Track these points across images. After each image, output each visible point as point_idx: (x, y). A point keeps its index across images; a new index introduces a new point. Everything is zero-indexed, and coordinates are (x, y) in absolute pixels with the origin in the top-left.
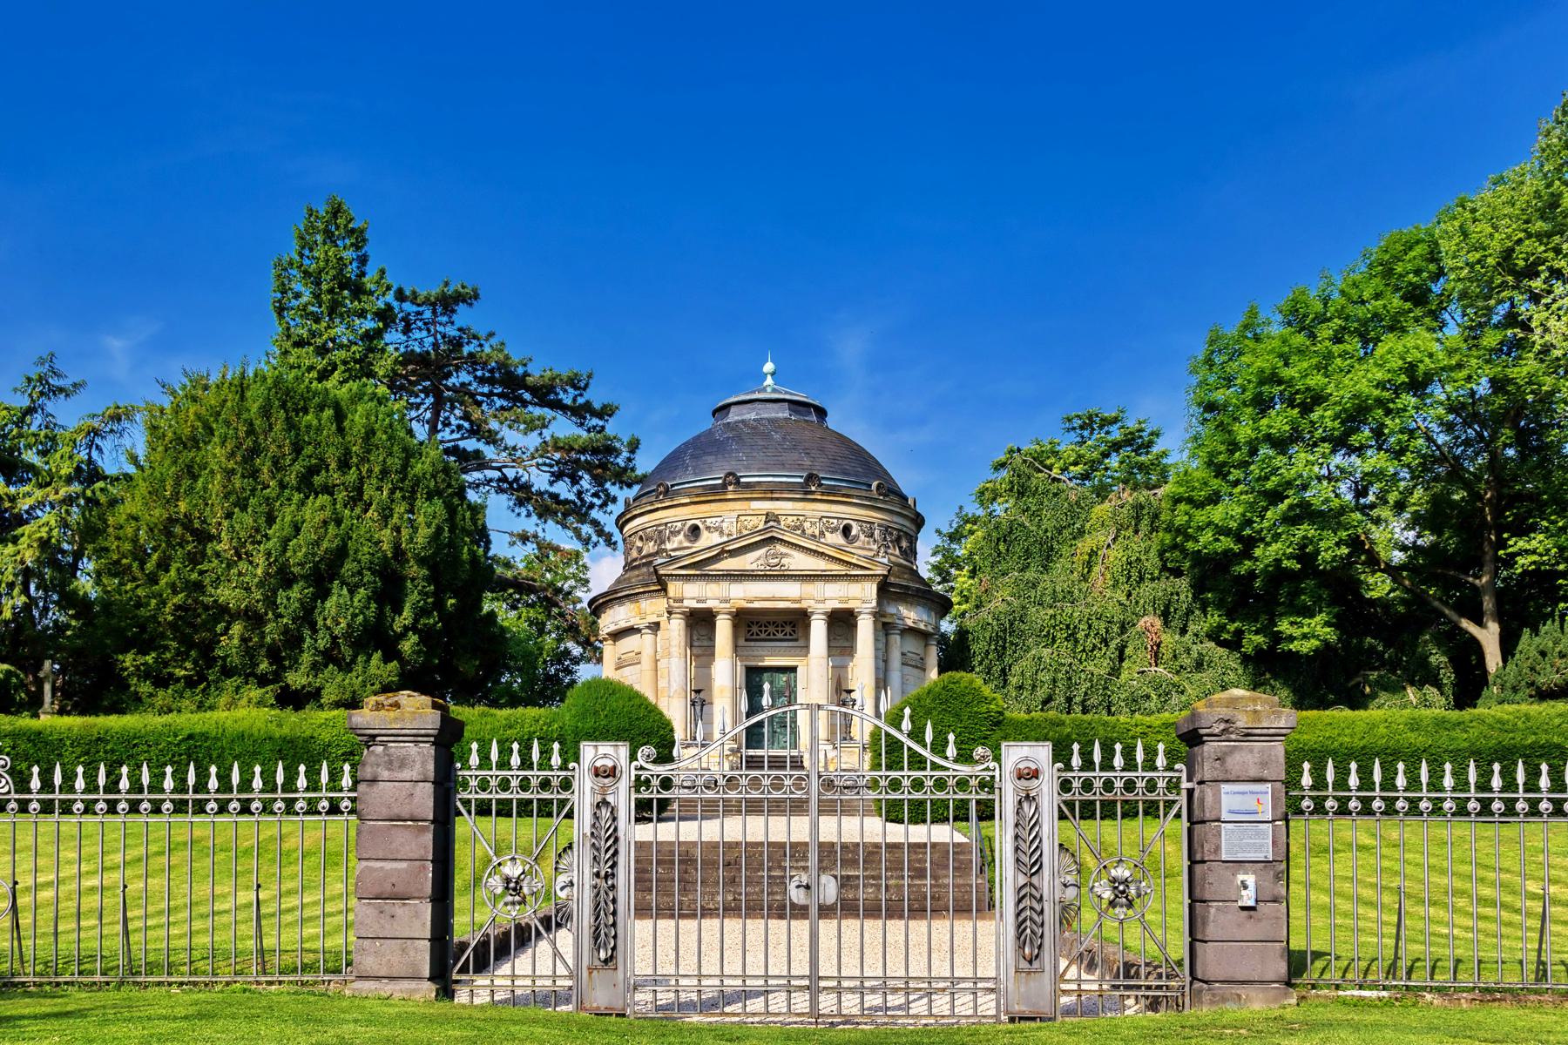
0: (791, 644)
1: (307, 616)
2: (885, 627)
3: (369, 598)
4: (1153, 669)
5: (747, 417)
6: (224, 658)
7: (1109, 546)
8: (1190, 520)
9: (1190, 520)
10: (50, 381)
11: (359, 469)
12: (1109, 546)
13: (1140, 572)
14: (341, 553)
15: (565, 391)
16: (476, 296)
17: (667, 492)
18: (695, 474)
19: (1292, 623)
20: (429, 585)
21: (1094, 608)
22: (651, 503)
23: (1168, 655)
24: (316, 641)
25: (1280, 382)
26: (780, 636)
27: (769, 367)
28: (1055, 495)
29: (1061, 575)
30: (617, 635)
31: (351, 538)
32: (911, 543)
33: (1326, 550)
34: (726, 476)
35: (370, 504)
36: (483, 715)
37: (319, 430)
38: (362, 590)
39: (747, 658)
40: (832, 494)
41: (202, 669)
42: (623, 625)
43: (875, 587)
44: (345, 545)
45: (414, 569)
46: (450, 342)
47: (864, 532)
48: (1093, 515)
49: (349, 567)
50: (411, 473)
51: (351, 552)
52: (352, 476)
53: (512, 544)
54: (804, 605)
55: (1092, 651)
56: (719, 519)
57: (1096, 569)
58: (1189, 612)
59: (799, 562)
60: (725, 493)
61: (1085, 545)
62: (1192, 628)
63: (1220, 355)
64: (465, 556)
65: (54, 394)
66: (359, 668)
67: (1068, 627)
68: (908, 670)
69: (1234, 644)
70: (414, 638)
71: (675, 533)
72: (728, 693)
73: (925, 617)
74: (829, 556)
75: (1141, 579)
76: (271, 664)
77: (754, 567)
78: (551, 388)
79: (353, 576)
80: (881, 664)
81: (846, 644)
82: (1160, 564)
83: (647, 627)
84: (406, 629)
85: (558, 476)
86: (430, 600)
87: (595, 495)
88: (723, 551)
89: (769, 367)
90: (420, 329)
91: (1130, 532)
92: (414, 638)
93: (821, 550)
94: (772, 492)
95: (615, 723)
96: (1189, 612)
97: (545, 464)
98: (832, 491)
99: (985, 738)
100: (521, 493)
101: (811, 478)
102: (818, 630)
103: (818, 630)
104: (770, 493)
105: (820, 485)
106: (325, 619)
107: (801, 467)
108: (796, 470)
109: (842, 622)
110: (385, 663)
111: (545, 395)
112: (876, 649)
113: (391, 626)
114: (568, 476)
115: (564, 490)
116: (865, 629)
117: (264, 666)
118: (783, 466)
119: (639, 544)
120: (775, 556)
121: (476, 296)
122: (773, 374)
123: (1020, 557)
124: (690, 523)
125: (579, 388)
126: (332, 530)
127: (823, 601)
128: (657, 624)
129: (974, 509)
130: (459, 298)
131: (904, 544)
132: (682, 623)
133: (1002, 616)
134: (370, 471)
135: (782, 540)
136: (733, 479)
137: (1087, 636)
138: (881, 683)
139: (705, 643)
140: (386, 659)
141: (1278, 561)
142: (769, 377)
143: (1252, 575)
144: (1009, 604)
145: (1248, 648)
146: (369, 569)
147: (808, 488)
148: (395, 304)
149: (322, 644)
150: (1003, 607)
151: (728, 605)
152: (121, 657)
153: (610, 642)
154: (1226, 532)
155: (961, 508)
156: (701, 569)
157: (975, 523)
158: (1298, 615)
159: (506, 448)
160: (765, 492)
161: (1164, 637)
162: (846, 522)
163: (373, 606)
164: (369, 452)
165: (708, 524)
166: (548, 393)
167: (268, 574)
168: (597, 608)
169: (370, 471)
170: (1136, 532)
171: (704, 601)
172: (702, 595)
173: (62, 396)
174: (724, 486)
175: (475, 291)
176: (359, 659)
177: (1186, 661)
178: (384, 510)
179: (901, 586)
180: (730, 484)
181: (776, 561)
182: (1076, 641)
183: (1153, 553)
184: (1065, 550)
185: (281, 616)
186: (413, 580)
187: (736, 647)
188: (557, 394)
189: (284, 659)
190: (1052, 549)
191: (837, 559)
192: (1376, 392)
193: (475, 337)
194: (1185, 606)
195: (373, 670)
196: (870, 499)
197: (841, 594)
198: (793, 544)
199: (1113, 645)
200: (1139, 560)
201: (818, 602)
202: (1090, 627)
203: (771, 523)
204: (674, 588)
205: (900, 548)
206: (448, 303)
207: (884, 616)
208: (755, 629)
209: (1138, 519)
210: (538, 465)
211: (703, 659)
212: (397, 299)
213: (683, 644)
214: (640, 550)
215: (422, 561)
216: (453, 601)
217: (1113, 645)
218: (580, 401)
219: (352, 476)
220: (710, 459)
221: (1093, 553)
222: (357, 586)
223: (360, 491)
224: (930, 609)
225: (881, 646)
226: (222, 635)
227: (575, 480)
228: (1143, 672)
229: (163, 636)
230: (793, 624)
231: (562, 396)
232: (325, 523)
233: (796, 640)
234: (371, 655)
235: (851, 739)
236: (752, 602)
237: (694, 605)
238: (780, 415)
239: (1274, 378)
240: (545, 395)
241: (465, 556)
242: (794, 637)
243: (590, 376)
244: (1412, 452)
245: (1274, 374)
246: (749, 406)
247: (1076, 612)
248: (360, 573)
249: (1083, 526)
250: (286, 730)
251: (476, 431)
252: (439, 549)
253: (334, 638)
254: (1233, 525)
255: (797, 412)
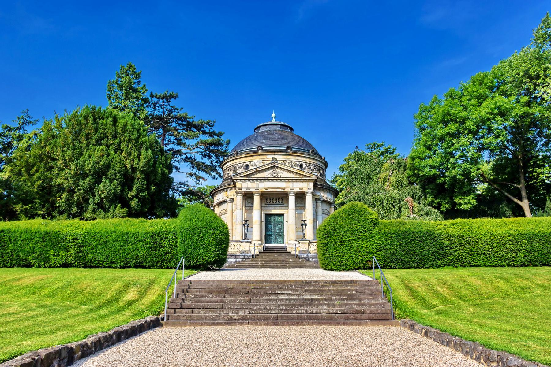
0: (282, 205)
1: (91, 190)
2: (316, 200)
3: (118, 184)
4: (412, 215)
5: (266, 130)
6: (59, 207)
7: (390, 176)
8: (420, 165)
9: (420, 165)
10: (27, 119)
11: (120, 138)
12: (390, 176)
13: (401, 184)
14: (108, 167)
15: (206, 127)
16: (177, 96)
17: (237, 153)
18: (247, 147)
19: (460, 199)
20: (145, 181)
21: (389, 195)
22: (232, 157)
23: (416, 211)
24: (94, 200)
25: (450, 115)
26: (278, 203)
27: (273, 115)
28: (370, 161)
29: (373, 185)
30: (219, 204)
31: (113, 162)
32: (324, 172)
33: (473, 172)
34: (258, 147)
35: (123, 151)
36: (142, 221)
37: (106, 124)
38: (115, 181)
39: (266, 211)
40: (296, 153)
41: (50, 211)
42: (221, 200)
43: (312, 184)
44: (110, 164)
45: (138, 175)
46: (169, 111)
47: (307, 167)
48: (383, 167)
49: (111, 172)
50: (140, 140)
51: (112, 167)
52: (117, 141)
53: (187, 177)
54: (286, 190)
55: (389, 209)
56: (256, 162)
57: (386, 183)
58: (421, 197)
59: (284, 175)
60: (258, 153)
61: (382, 176)
62: (422, 202)
63: (426, 112)
64: (160, 171)
65: (28, 123)
66: (111, 211)
67: (380, 201)
68: (324, 215)
69: (438, 207)
70: (136, 200)
71: (240, 167)
72: (258, 223)
73: (330, 197)
74: (295, 172)
75: (402, 187)
76: (77, 209)
77: (268, 176)
78: (202, 126)
79: (112, 175)
80: (315, 213)
81: (302, 205)
82: (408, 182)
83: (230, 200)
84: (133, 197)
85: (205, 156)
86: (145, 187)
87: (217, 162)
88: (256, 171)
89: (273, 115)
90: (159, 107)
91: (397, 171)
92: (136, 200)
93: (292, 170)
94: (274, 152)
95: (199, 224)
96: (421, 197)
97: (200, 152)
98: (295, 152)
99: (371, 230)
100: (191, 161)
101: (288, 147)
102: (292, 199)
103: (292, 199)
104: (274, 152)
105: (291, 150)
106: (99, 191)
107: (284, 144)
108: (282, 145)
109: (300, 197)
110: (122, 209)
111: (199, 128)
112: (313, 208)
113: (127, 195)
114: (208, 156)
115: (207, 161)
116: (309, 199)
117: (74, 210)
118: (278, 144)
119: (228, 172)
120: (275, 173)
121: (177, 96)
122: (275, 118)
123: (360, 180)
124: (245, 164)
125: (211, 126)
126: (105, 158)
127: (293, 189)
128: (233, 199)
129: (339, 173)
130: (171, 96)
131: (321, 172)
132: (241, 197)
133: (356, 198)
134: (124, 139)
135: (278, 167)
136: (261, 148)
137: (387, 204)
138: (315, 220)
139: (250, 205)
140: (122, 207)
141: (455, 176)
142: (274, 118)
143: (444, 183)
144: (358, 194)
145: (443, 209)
146: (119, 173)
147: (288, 151)
148: (150, 98)
149: (96, 201)
150: (356, 195)
151: (258, 190)
152: (15, 206)
153: (217, 207)
154: (433, 167)
155: (335, 173)
156: (248, 178)
157: (339, 177)
158: (462, 196)
159: (186, 146)
160: (272, 152)
161: (414, 204)
162: (301, 163)
163: (120, 187)
164: (124, 132)
165: (252, 164)
166: (201, 128)
167: (76, 173)
168: (213, 194)
169: (124, 139)
170: (399, 171)
171: (249, 189)
172: (249, 187)
173: (31, 124)
174: (258, 150)
175: (177, 95)
176: (112, 207)
177: (423, 213)
178: (128, 153)
179: (321, 185)
180: (260, 150)
181: (276, 174)
182: (383, 206)
183: (405, 178)
184: (375, 178)
185: (80, 190)
186: (138, 179)
187: (261, 207)
188: (204, 128)
189: (83, 207)
190: (370, 177)
191: (298, 173)
192: (488, 115)
193: (176, 109)
194: (419, 195)
195: (116, 211)
196: (310, 155)
197: (300, 186)
198: (282, 168)
199: (397, 207)
200: (401, 180)
201: (291, 189)
202: (388, 201)
203: (274, 161)
204: (238, 185)
205: (320, 173)
206: (168, 98)
207: (315, 196)
208: (268, 200)
209: (399, 167)
210: (197, 152)
211: (250, 211)
212: (150, 96)
213: (241, 205)
214: (228, 174)
215: (142, 172)
216: (154, 188)
217: (397, 207)
218: (211, 130)
219: (117, 141)
220: (253, 142)
221: (385, 178)
222: (114, 179)
223: (119, 145)
224: (332, 194)
225: (315, 206)
226: (58, 198)
227: (210, 157)
228: (409, 216)
229: (35, 198)
230: (282, 198)
231: (205, 129)
232: (103, 156)
233: (284, 204)
234: (117, 206)
235: (305, 239)
236: (267, 189)
237: (246, 190)
238: (277, 129)
239: (448, 114)
240: (199, 128)
241: (160, 171)
242: (283, 203)
243: (214, 122)
244: (503, 136)
245: (448, 112)
246: (267, 126)
247: (382, 196)
248: (115, 175)
249: (380, 170)
250: (48, 229)
251: (179, 143)
252: (149, 167)
253: (102, 199)
254: (437, 165)
255: (283, 128)
